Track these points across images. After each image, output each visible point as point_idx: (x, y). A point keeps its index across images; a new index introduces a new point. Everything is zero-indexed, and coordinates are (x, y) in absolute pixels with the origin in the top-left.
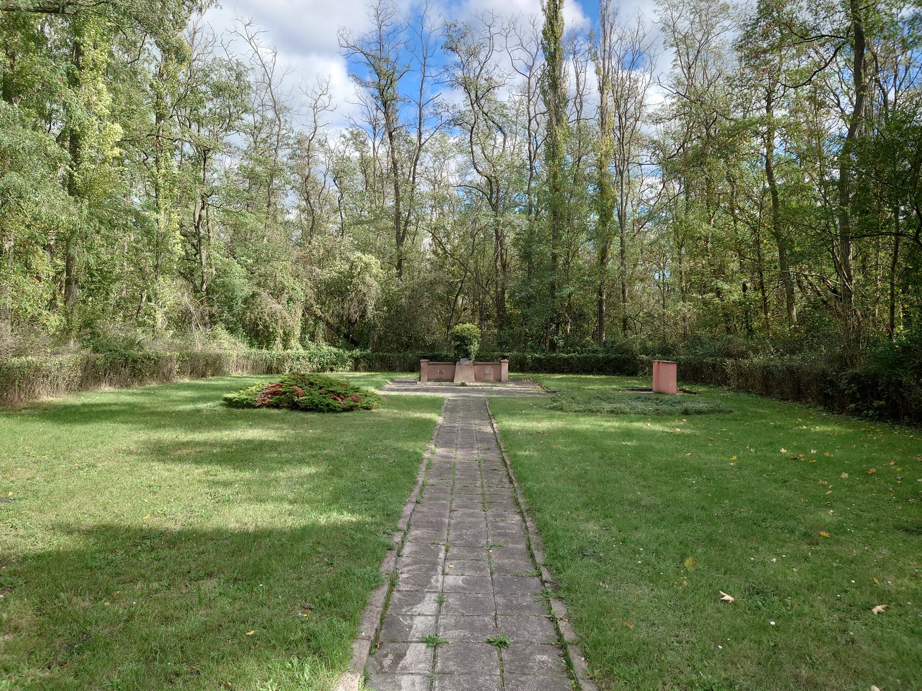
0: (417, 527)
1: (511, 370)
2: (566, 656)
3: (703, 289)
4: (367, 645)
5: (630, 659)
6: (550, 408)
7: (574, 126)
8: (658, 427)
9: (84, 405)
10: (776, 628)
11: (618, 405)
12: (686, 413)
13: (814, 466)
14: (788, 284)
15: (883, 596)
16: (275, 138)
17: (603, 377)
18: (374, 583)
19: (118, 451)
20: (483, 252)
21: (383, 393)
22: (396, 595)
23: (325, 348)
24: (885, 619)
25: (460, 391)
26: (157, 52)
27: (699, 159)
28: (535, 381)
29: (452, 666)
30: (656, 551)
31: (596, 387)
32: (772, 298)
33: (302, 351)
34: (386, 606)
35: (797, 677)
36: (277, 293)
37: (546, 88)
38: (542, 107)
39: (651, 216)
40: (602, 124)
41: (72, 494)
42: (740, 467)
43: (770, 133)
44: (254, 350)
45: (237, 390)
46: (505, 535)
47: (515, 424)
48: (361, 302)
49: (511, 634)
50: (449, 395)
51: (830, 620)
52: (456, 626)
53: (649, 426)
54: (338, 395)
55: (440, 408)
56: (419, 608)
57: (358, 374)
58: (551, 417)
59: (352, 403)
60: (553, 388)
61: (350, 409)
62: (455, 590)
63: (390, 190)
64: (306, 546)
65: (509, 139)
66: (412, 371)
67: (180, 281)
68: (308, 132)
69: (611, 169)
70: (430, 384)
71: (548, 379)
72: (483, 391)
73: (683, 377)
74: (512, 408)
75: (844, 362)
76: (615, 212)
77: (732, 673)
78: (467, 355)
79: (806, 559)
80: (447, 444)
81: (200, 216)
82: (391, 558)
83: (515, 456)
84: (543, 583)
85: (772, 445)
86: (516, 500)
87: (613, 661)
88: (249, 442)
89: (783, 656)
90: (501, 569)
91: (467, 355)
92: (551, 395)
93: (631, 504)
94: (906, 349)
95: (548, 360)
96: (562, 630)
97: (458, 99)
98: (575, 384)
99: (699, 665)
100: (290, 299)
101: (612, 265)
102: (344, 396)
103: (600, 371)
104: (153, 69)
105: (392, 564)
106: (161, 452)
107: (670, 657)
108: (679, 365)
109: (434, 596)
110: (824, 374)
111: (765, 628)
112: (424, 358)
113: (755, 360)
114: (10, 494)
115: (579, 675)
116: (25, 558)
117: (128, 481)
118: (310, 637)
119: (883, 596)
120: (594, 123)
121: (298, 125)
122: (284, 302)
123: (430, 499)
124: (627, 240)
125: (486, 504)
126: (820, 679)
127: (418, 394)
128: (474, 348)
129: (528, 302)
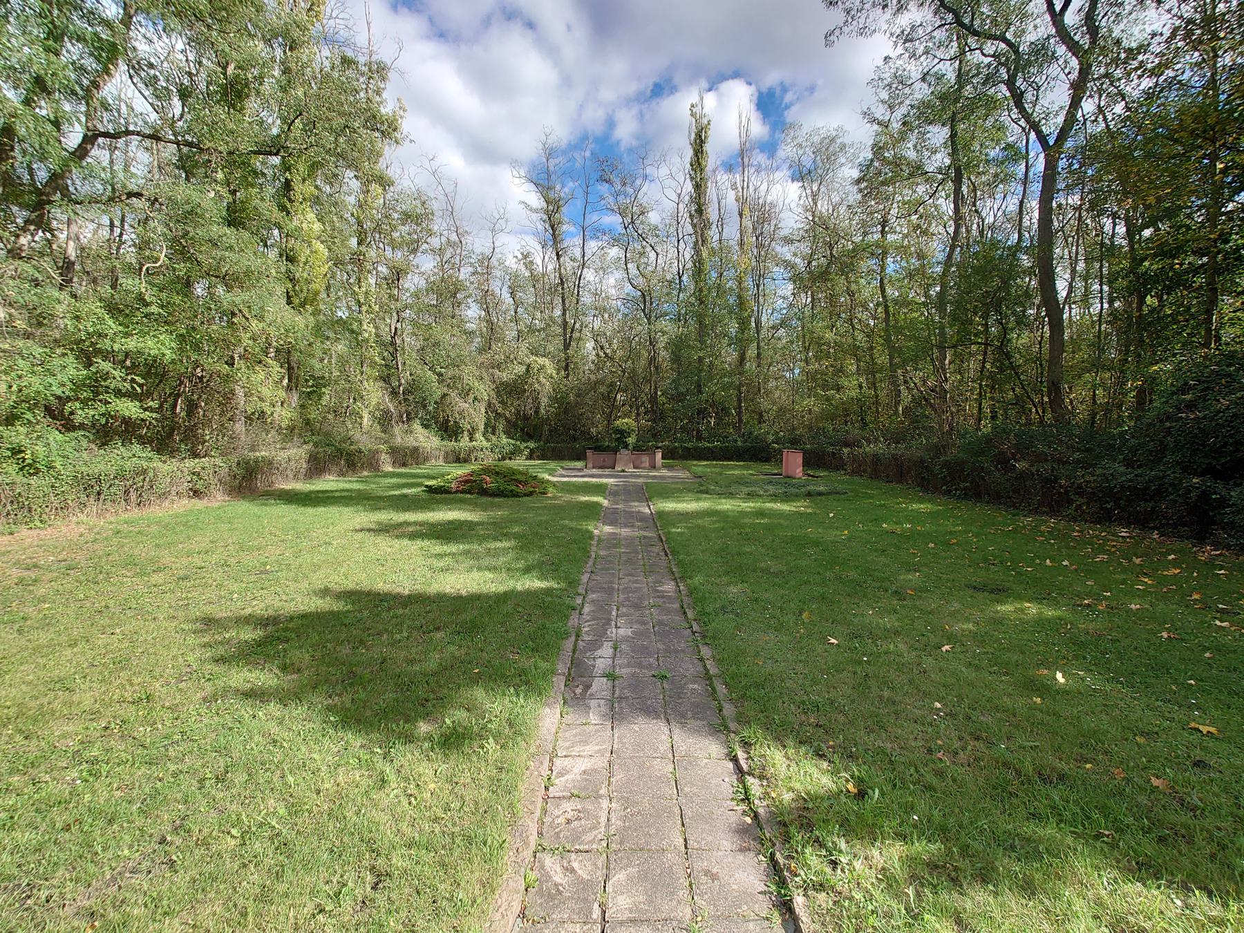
0: (593, 592)
1: (663, 458)
2: (711, 685)
3: (825, 387)
4: (563, 678)
5: (758, 686)
6: (697, 492)
7: (715, 245)
8: (785, 507)
9: (311, 492)
10: (868, 662)
11: (753, 489)
12: (809, 494)
13: (908, 538)
14: (895, 384)
15: (951, 638)
16: (458, 258)
17: (741, 463)
18: (567, 635)
19: (346, 530)
20: (639, 355)
21: (555, 479)
22: (581, 643)
23: (505, 440)
24: (951, 655)
25: (621, 477)
26: (355, 184)
27: (823, 276)
28: (684, 468)
29: (627, 693)
30: (781, 608)
31: (736, 472)
32: (882, 394)
33: (485, 443)
34: (574, 651)
35: (881, 697)
36: (465, 393)
37: (693, 212)
38: (689, 229)
39: (783, 324)
40: (741, 244)
41: (316, 567)
42: (849, 539)
43: (885, 253)
44: (445, 443)
45: (433, 478)
46: (663, 597)
47: (670, 506)
48: (536, 400)
49: (670, 670)
50: (611, 481)
51: (910, 656)
52: (628, 665)
53: (778, 506)
54: (520, 482)
55: (604, 492)
56: (599, 653)
57: (532, 462)
58: (698, 500)
59: (531, 489)
60: (700, 474)
61: (530, 494)
62: (626, 639)
63: (558, 300)
64: (508, 607)
65: (660, 256)
66: (579, 459)
67: (381, 384)
68: (488, 252)
69: (749, 283)
70: (595, 471)
71: (695, 465)
72: (640, 476)
73: (807, 463)
74: (666, 492)
75: (939, 450)
76: (753, 319)
77: (833, 694)
78: (626, 446)
79: (895, 611)
80: (612, 523)
81: (396, 329)
82: (575, 615)
83: (669, 533)
84: (694, 633)
85: (877, 521)
86: (671, 569)
87: (747, 687)
88: (451, 522)
89: (871, 683)
90: (660, 623)
91: (626, 446)
92: (699, 480)
93: (762, 571)
94: (988, 440)
95: (696, 449)
96: (708, 667)
97: (613, 220)
98: (718, 470)
99: (809, 689)
100: (475, 398)
101: (750, 366)
102: (525, 483)
103: (739, 458)
104: (351, 200)
105: (576, 620)
106: (384, 529)
107: (789, 683)
108: (805, 453)
109: (610, 644)
110: (922, 461)
111: (860, 662)
112: (590, 449)
113: (868, 449)
114: (268, 567)
115: (722, 697)
116: (292, 618)
117: (359, 556)
118: (523, 672)
119: (951, 638)
120: (734, 243)
121: (478, 244)
122: (471, 401)
123: (602, 569)
124: (762, 344)
125: (649, 572)
126: (897, 699)
127: (586, 479)
128: (631, 440)
129: (679, 398)
